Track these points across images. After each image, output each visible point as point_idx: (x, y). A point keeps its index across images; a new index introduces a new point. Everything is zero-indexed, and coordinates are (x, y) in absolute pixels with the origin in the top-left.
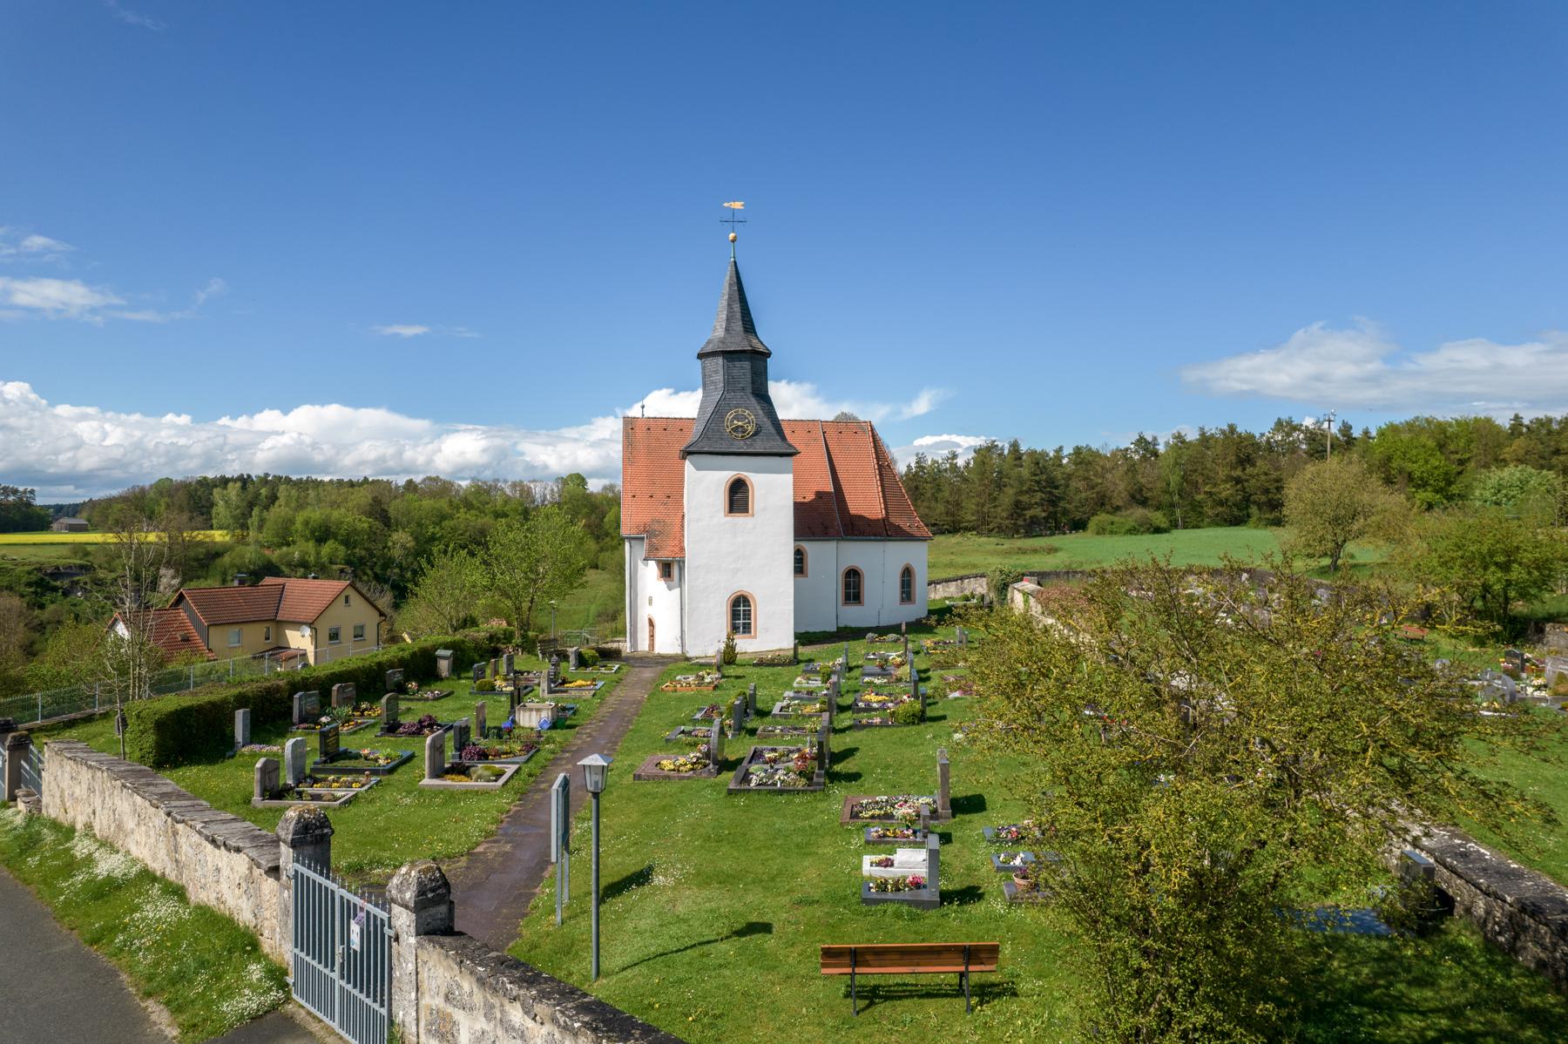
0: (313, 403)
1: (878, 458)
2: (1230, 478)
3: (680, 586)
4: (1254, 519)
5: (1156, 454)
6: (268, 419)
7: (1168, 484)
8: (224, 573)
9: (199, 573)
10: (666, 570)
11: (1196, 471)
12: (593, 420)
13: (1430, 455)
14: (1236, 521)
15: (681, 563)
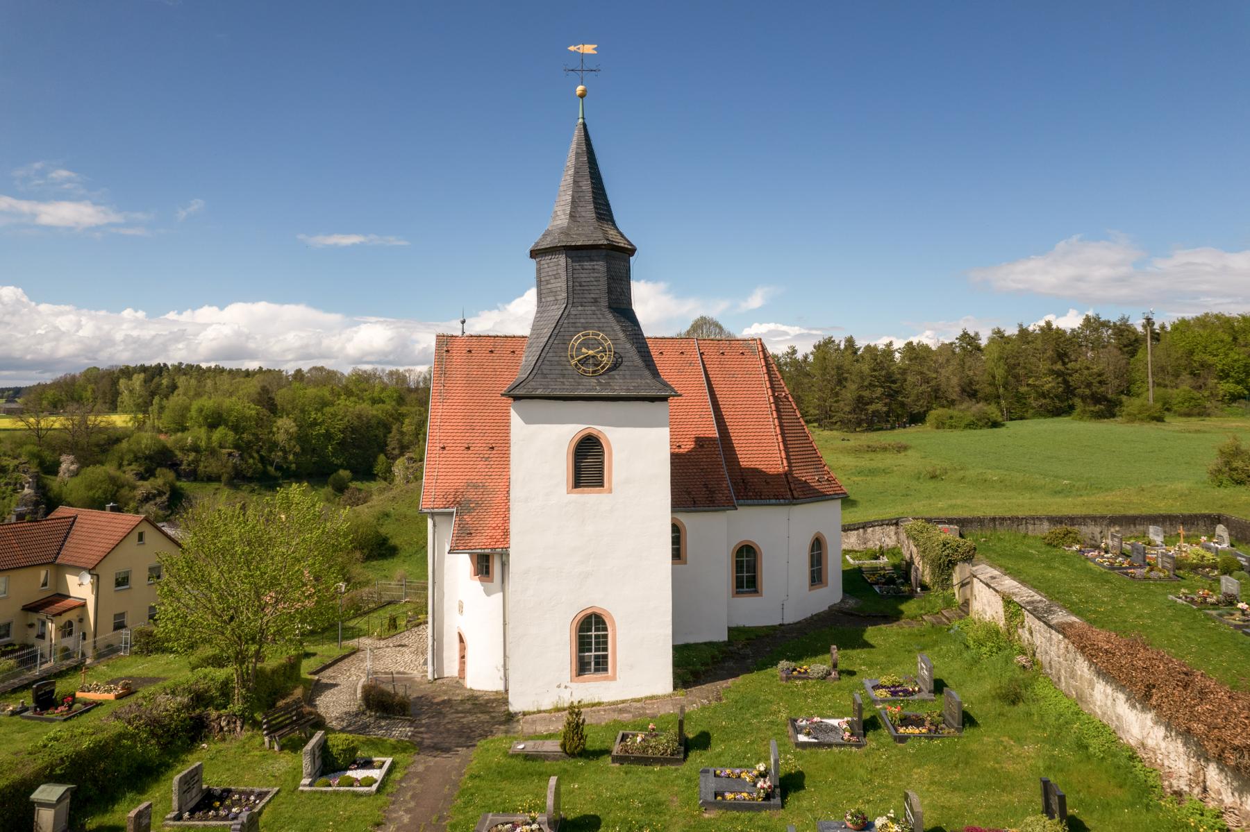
0: (245, 301)
1: (773, 388)
2: (1052, 372)
3: (503, 590)
4: (1078, 410)
5: (978, 348)
6: (207, 313)
7: (994, 377)
8: (122, 459)
9: (100, 457)
10: (483, 565)
11: (1019, 364)
12: (480, 313)
13: (1229, 349)
14: (1057, 413)
15: (504, 556)
